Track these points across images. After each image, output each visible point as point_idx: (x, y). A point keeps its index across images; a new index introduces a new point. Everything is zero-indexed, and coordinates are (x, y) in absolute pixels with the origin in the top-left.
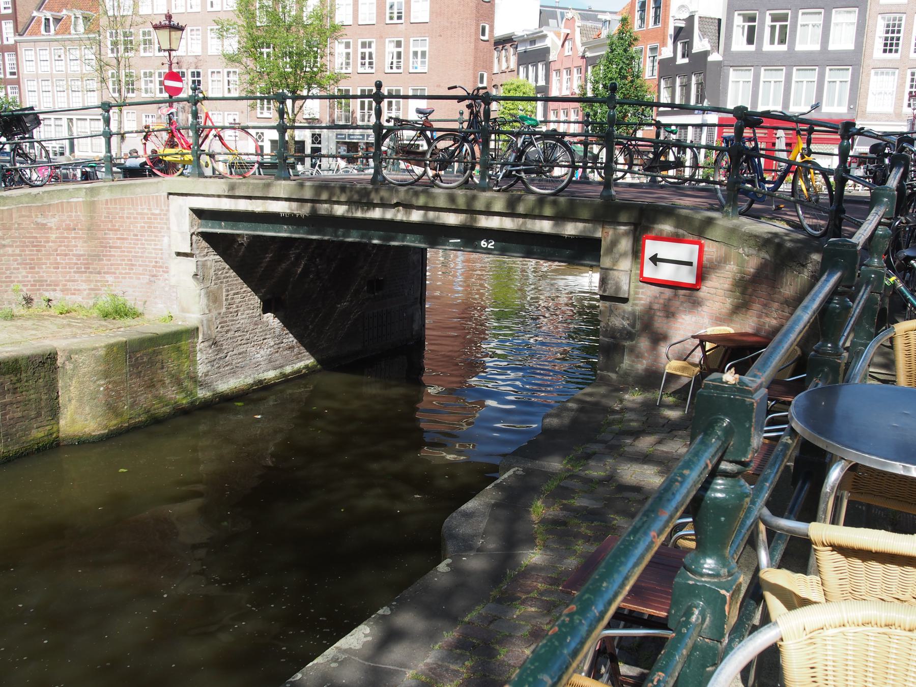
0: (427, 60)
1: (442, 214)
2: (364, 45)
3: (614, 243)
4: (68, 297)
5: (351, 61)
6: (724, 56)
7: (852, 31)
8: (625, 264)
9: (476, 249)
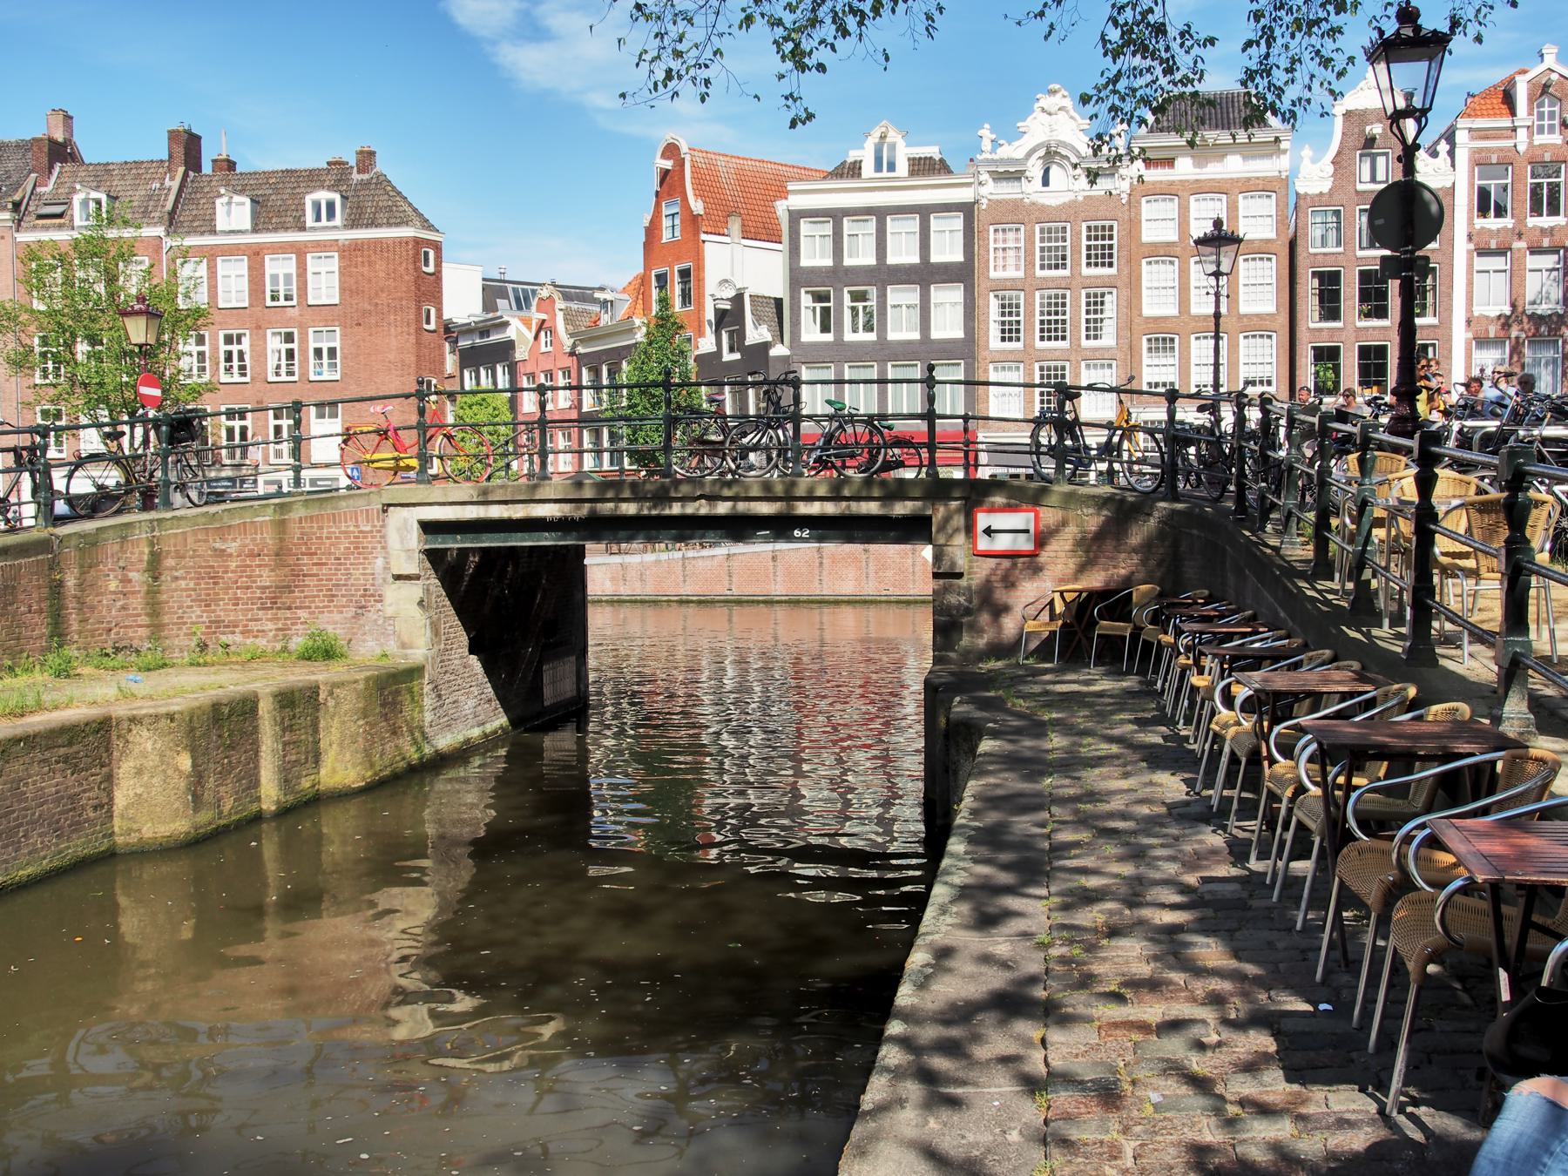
0: (338, 361)
1: (753, 504)
2: (229, 340)
3: (947, 520)
4: (248, 641)
5: (207, 364)
6: (791, 348)
7: (959, 313)
8: (960, 539)
9: (790, 539)
